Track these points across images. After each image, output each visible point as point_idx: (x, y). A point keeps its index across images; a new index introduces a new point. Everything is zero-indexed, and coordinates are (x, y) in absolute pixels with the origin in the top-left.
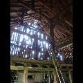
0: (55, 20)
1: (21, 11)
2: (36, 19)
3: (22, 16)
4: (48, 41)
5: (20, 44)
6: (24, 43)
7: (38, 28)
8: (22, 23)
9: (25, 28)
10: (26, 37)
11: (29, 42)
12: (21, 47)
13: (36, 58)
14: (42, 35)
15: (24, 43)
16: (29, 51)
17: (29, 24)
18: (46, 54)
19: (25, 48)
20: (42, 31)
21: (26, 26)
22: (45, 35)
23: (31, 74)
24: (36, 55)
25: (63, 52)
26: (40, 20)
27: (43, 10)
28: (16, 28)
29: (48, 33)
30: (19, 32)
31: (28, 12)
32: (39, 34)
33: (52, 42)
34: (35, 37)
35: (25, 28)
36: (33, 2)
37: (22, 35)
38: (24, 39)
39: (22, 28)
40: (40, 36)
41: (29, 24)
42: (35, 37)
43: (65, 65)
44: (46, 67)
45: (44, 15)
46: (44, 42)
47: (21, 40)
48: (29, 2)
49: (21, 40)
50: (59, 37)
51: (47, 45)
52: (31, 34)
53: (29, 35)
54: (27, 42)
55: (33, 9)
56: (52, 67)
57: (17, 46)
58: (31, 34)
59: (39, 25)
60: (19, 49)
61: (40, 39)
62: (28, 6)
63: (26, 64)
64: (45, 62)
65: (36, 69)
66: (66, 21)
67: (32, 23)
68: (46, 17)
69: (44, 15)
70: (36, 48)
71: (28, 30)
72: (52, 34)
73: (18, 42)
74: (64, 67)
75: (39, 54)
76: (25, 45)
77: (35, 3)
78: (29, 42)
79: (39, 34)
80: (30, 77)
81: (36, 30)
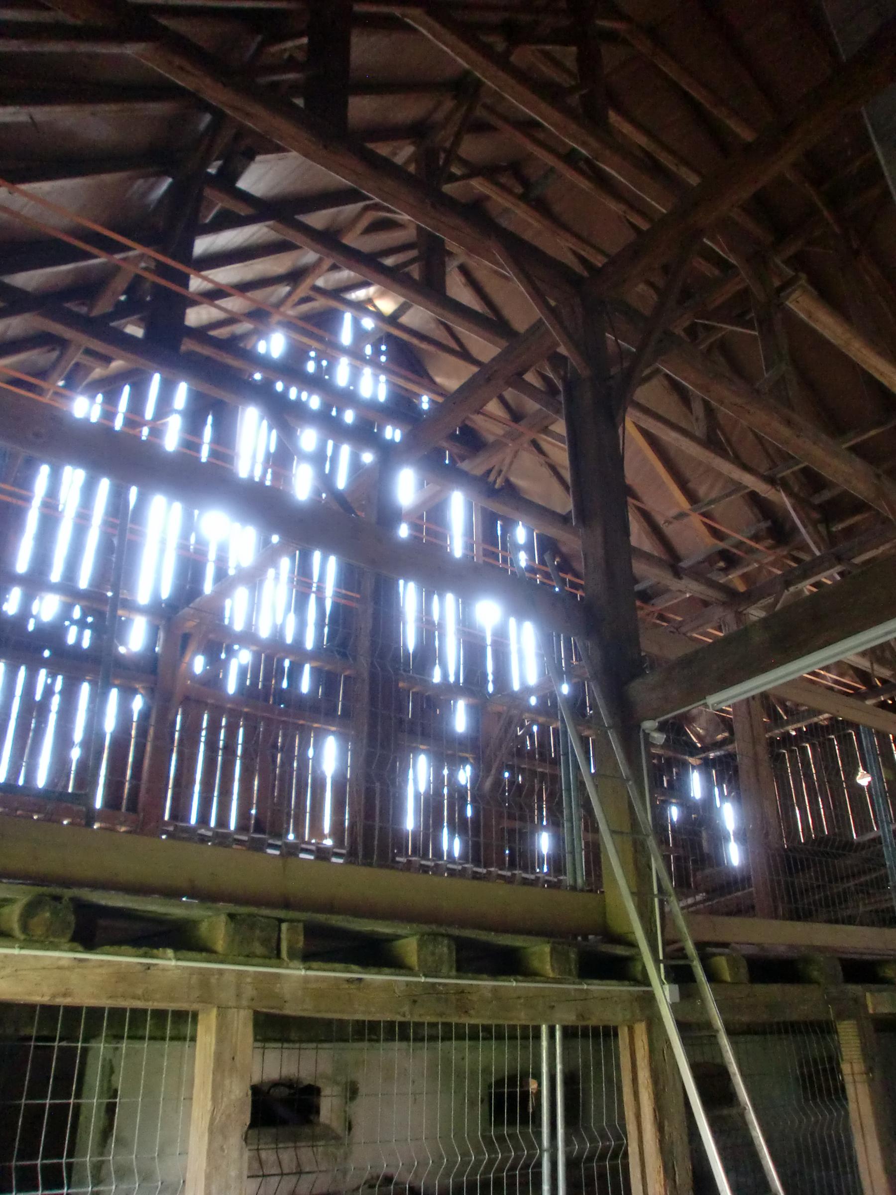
0: (641, 294)
1: (154, 157)
2: (371, 265)
3: (171, 230)
4: (524, 594)
5: (136, 638)
6: (189, 617)
7: (400, 408)
8: (168, 341)
9: (212, 407)
10: (231, 536)
11: (275, 605)
12: (151, 673)
13: (370, 833)
14: (458, 507)
15: (189, 617)
16: (271, 717)
17: (274, 344)
18: (519, 771)
19: (204, 696)
20: (452, 443)
21: (221, 373)
22: (500, 497)
23: (277, 1064)
24: (372, 790)
25: (765, 755)
26: (427, 285)
27: (473, 148)
28: (85, 408)
29: (542, 466)
30: (122, 457)
31: (258, 178)
32: (407, 487)
33: (601, 607)
34: (352, 527)
35: (212, 407)
36: (329, 46)
37: (163, 518)
38: (191, 568)
39: (166, 410)
40: (432, 516)
41: (274, 344)
42: (352, 527)
43: (779, 935)
44: (509, 963)
45: (475, 213)
46: (489, 612)
47: (154, 577)
48: (268, 24)
49: (154, 577)
50: (693, 538)
51: (526, 654)
52: (303, 485)
53: (264, 504)
54: (236, 611)
55: (326, 126)
56: (606, 961)
57: (96, 665)
58: (303, 485)
59: (406, 355)
60: (116, 711)
61: (429, 563)
62: (276, 99)
63: (215, 926)
64: (495, 896)
65: (376, 991)
66: (802, 304)
67: (318, 325)
68: (522, 255)
69: (475, 213)
70: (377, 689)
71: (253, 436)
72: (599, 490)
73: (104, 604)
74: (767, 969)
75: (419, 774)
76: (217, 642)
77: (365, 50)
78: (275, 605)
79: (407, 487)
80: (279, 1112)
81: (364, 434)
